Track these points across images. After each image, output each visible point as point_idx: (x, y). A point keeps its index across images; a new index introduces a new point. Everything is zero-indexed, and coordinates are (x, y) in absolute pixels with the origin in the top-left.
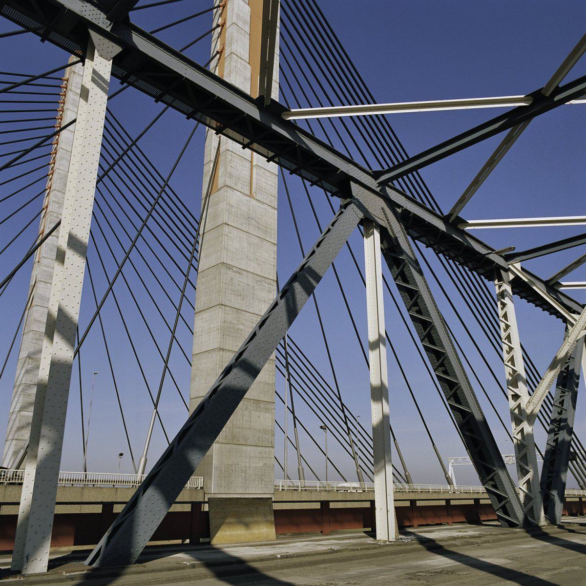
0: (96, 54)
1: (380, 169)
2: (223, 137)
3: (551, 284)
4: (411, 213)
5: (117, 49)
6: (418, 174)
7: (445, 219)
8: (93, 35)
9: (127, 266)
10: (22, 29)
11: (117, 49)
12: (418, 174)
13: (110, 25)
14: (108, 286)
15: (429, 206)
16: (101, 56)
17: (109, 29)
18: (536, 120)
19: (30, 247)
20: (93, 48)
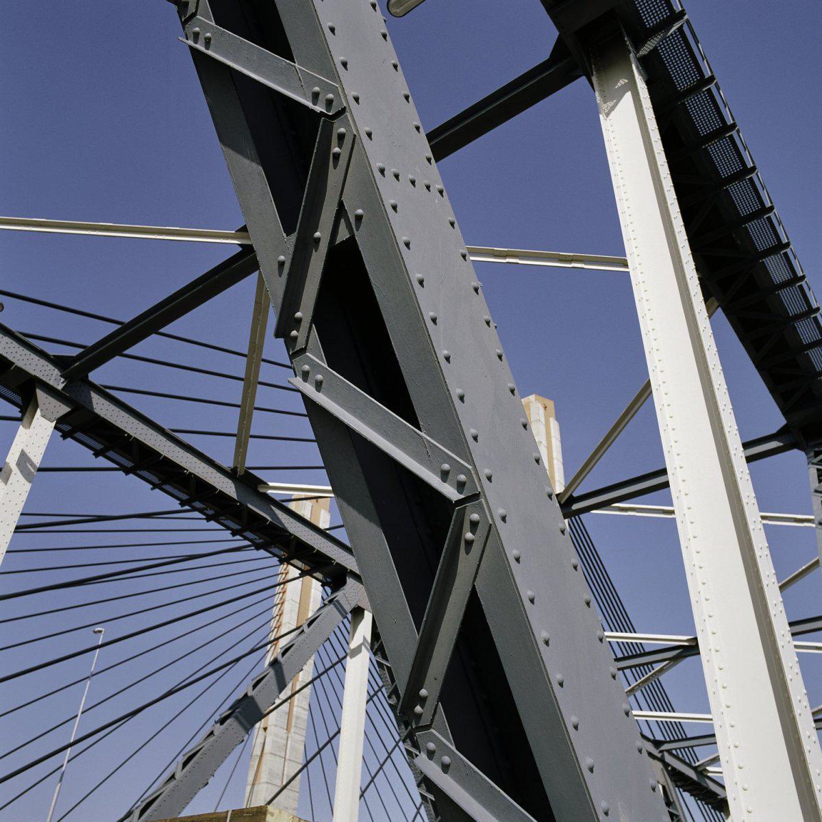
0: (39, 412)
1: (663, 739)
2: (290, 567)
3: (700, 769)
4: (216, 489)
5: (64, 409)
6: (693, 750)
7: (231, 474)
8: (40, 394)
9: (380, 779)
10: (271, 555)
11: (64, 409)
12: (693, 750)
13: (63, 383)
14: (416, 810)
15: (687, 761)
16: (43, 416)
17: (60, 387)
18: (688, 658)
19: (128, 722)
20: (36, 406)
